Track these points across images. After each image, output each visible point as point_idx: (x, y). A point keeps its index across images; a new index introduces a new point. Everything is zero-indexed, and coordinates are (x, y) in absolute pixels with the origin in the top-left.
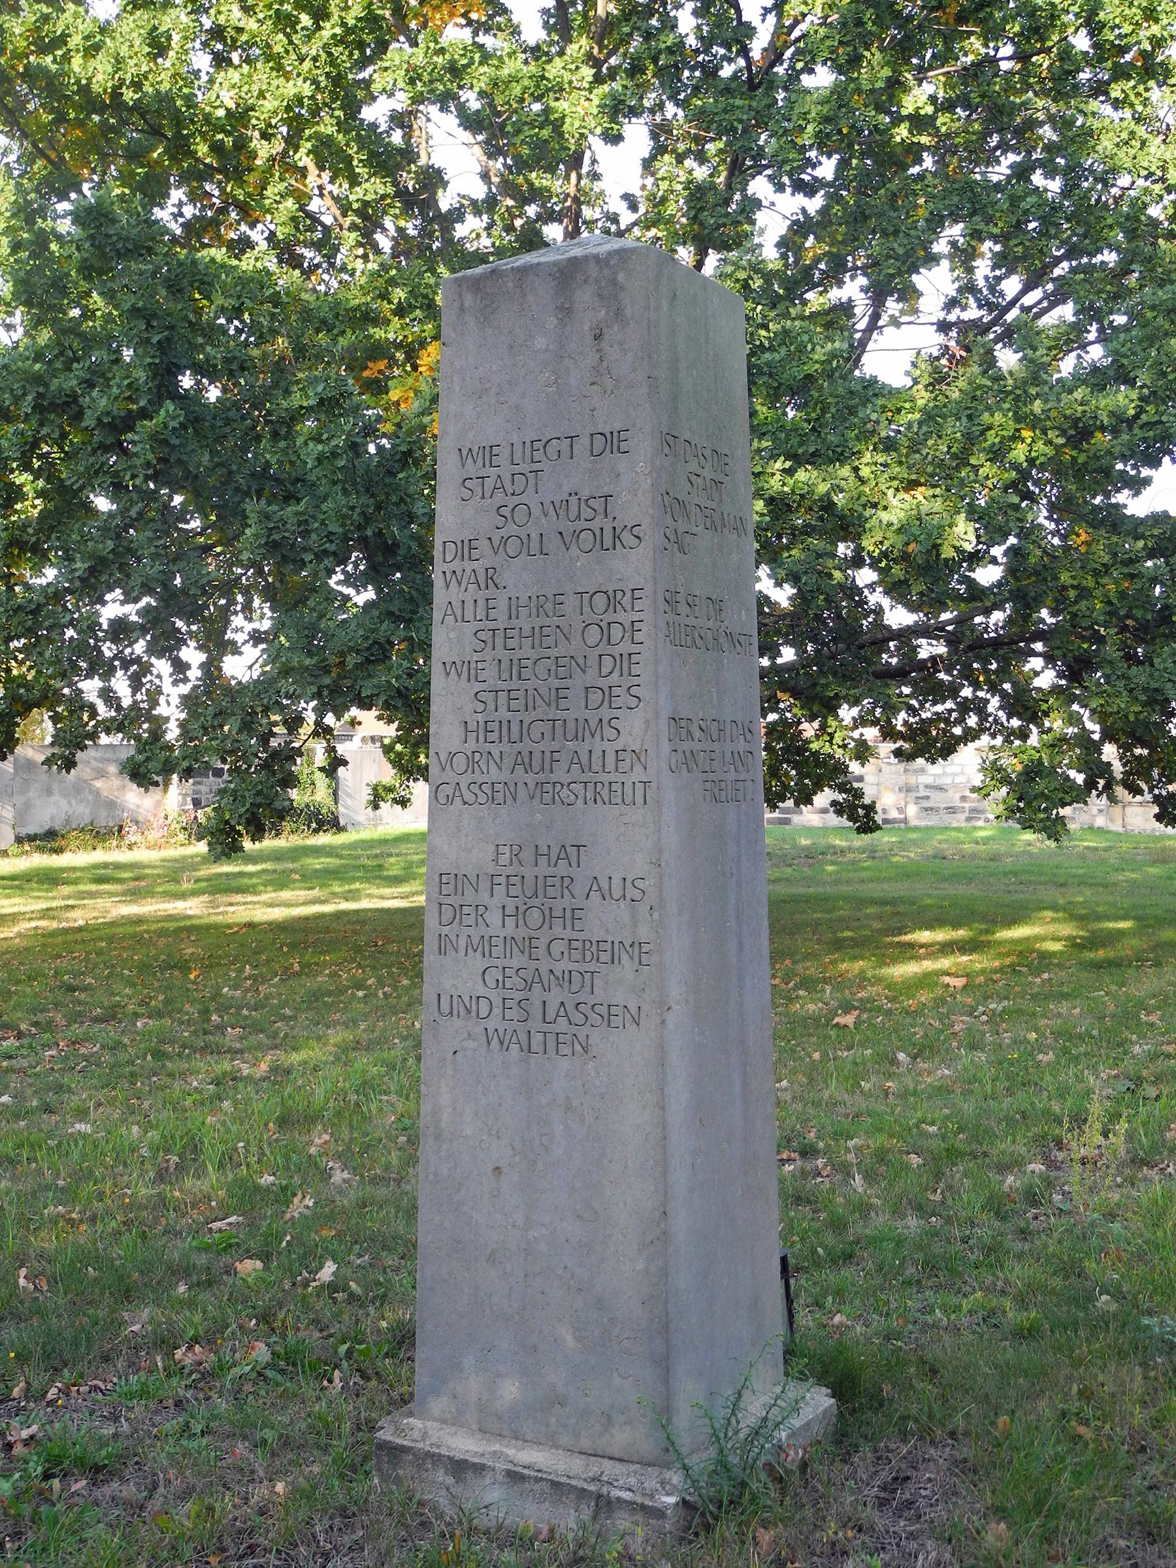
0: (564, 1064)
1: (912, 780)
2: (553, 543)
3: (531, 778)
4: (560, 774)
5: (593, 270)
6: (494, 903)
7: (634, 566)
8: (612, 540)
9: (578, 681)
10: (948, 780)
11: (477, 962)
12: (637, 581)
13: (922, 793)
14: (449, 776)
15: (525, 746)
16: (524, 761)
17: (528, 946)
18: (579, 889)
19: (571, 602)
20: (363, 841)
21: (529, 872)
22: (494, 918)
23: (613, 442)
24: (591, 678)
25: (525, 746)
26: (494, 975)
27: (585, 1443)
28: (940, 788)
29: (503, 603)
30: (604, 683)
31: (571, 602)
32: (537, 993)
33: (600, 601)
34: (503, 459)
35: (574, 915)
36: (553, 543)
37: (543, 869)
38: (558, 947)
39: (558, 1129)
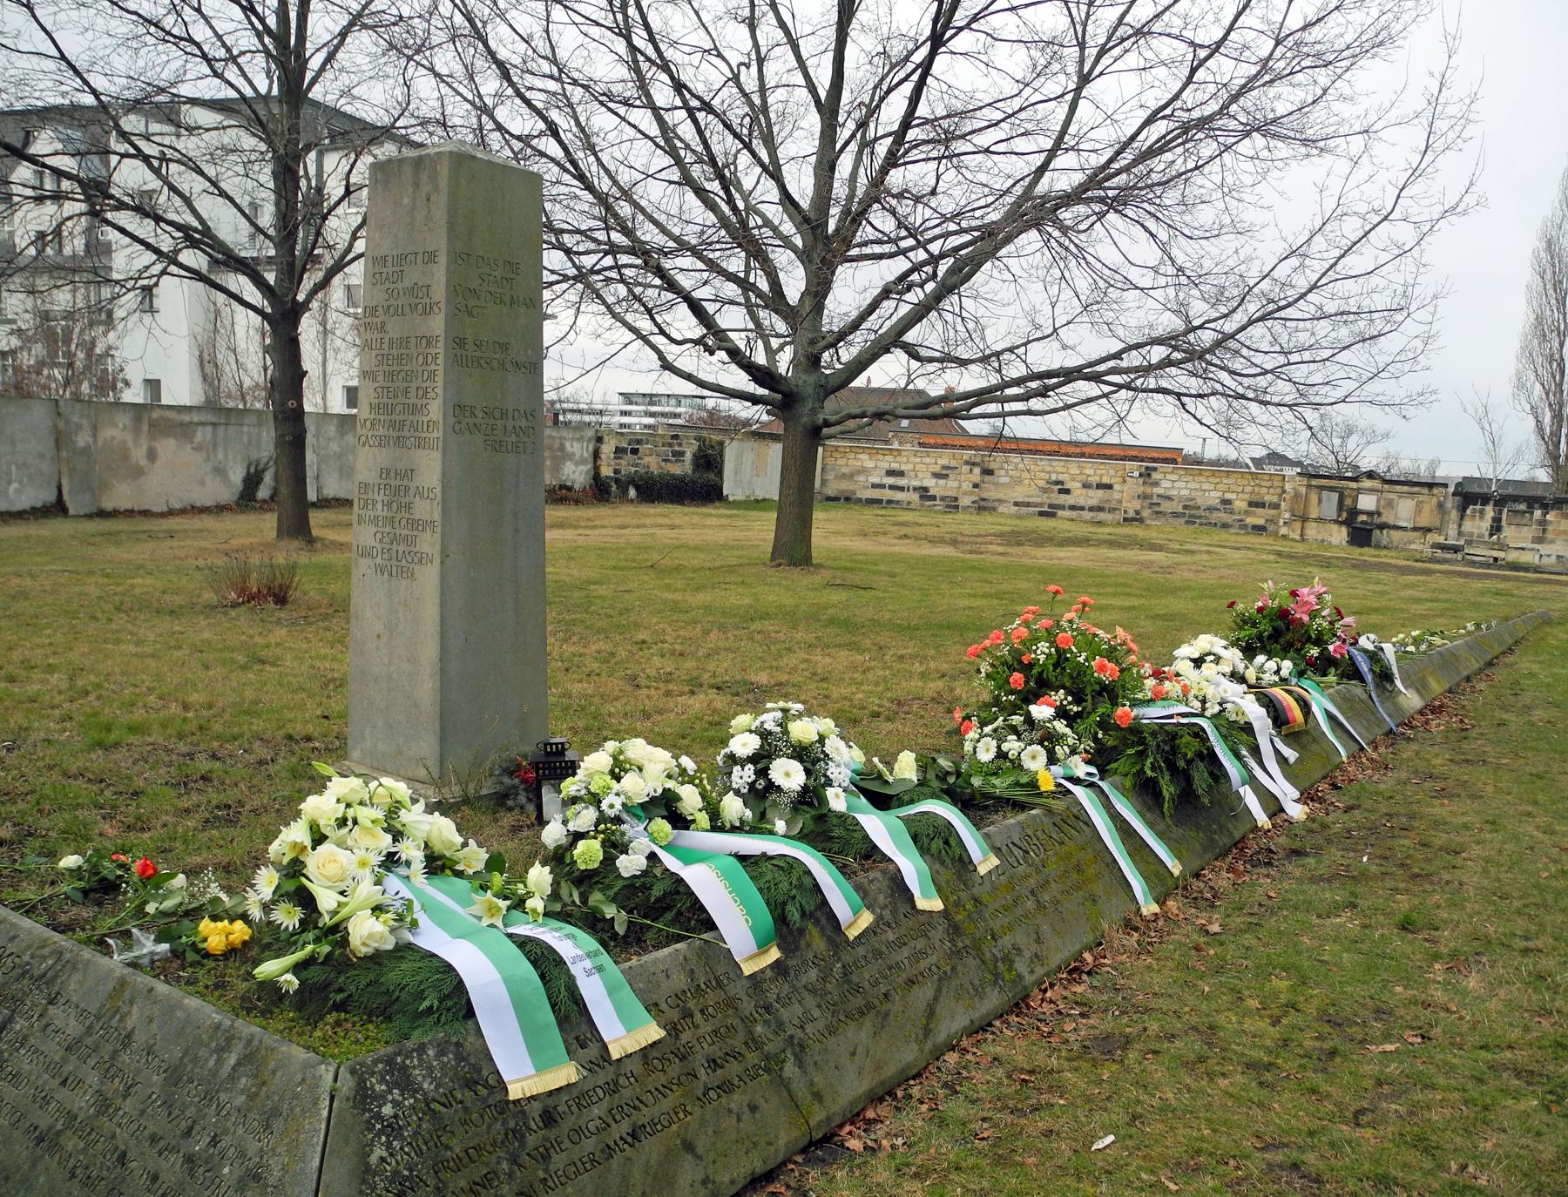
0: (404, 582)
1: (1148, 490)
2: (407, 309)
3: (395, 434)
4: (406, 433)
5: (427, 162)
6: (379, 498)
7: (437, 324)
8: (428, 311)
9: (414, 385)
10: (1175, 492)
11: (373, 529)
12: (438, 332)
13: (1155, 500)
14: (364, 431)
15: (394, 417)
16: (393, 425)
17: (391, 521)
18: (412, 492)
19: (413, 341)
20: (892, 555)
21: (393, 482)
22: (379, 506)
23: (432, 257)
24: (419, 383)
25: (394, 417)
26: (379, 536)
27: (410, 774)
28: (1169, 498)
29: (386, 341)
30: (424, 385)
31: (413, 341)
32: (395, 546)
33: (424, 342)
34: (389, 264)
35: (409, 506)
36: (407, 309)
37: (398, 482)
38: (403, 522)
39: (401, 616)
